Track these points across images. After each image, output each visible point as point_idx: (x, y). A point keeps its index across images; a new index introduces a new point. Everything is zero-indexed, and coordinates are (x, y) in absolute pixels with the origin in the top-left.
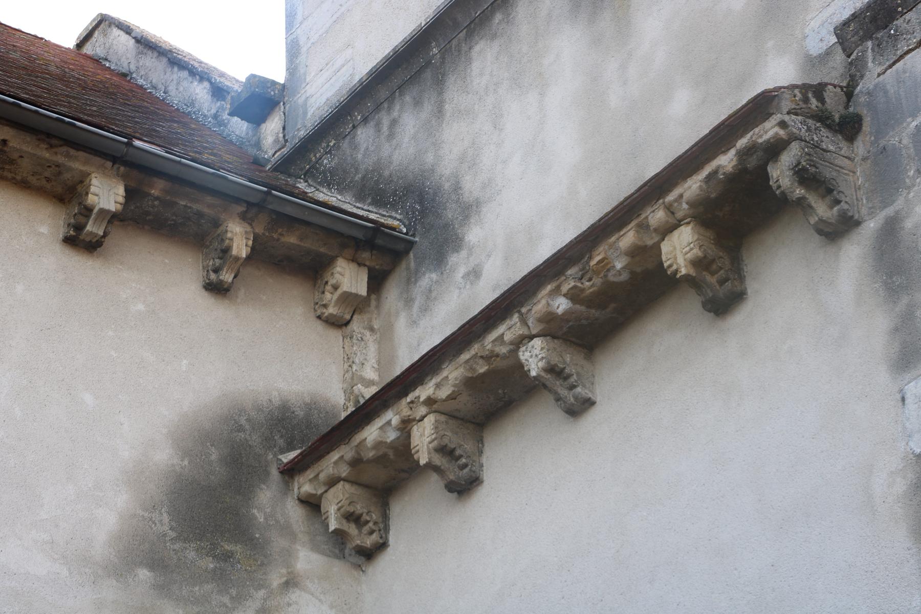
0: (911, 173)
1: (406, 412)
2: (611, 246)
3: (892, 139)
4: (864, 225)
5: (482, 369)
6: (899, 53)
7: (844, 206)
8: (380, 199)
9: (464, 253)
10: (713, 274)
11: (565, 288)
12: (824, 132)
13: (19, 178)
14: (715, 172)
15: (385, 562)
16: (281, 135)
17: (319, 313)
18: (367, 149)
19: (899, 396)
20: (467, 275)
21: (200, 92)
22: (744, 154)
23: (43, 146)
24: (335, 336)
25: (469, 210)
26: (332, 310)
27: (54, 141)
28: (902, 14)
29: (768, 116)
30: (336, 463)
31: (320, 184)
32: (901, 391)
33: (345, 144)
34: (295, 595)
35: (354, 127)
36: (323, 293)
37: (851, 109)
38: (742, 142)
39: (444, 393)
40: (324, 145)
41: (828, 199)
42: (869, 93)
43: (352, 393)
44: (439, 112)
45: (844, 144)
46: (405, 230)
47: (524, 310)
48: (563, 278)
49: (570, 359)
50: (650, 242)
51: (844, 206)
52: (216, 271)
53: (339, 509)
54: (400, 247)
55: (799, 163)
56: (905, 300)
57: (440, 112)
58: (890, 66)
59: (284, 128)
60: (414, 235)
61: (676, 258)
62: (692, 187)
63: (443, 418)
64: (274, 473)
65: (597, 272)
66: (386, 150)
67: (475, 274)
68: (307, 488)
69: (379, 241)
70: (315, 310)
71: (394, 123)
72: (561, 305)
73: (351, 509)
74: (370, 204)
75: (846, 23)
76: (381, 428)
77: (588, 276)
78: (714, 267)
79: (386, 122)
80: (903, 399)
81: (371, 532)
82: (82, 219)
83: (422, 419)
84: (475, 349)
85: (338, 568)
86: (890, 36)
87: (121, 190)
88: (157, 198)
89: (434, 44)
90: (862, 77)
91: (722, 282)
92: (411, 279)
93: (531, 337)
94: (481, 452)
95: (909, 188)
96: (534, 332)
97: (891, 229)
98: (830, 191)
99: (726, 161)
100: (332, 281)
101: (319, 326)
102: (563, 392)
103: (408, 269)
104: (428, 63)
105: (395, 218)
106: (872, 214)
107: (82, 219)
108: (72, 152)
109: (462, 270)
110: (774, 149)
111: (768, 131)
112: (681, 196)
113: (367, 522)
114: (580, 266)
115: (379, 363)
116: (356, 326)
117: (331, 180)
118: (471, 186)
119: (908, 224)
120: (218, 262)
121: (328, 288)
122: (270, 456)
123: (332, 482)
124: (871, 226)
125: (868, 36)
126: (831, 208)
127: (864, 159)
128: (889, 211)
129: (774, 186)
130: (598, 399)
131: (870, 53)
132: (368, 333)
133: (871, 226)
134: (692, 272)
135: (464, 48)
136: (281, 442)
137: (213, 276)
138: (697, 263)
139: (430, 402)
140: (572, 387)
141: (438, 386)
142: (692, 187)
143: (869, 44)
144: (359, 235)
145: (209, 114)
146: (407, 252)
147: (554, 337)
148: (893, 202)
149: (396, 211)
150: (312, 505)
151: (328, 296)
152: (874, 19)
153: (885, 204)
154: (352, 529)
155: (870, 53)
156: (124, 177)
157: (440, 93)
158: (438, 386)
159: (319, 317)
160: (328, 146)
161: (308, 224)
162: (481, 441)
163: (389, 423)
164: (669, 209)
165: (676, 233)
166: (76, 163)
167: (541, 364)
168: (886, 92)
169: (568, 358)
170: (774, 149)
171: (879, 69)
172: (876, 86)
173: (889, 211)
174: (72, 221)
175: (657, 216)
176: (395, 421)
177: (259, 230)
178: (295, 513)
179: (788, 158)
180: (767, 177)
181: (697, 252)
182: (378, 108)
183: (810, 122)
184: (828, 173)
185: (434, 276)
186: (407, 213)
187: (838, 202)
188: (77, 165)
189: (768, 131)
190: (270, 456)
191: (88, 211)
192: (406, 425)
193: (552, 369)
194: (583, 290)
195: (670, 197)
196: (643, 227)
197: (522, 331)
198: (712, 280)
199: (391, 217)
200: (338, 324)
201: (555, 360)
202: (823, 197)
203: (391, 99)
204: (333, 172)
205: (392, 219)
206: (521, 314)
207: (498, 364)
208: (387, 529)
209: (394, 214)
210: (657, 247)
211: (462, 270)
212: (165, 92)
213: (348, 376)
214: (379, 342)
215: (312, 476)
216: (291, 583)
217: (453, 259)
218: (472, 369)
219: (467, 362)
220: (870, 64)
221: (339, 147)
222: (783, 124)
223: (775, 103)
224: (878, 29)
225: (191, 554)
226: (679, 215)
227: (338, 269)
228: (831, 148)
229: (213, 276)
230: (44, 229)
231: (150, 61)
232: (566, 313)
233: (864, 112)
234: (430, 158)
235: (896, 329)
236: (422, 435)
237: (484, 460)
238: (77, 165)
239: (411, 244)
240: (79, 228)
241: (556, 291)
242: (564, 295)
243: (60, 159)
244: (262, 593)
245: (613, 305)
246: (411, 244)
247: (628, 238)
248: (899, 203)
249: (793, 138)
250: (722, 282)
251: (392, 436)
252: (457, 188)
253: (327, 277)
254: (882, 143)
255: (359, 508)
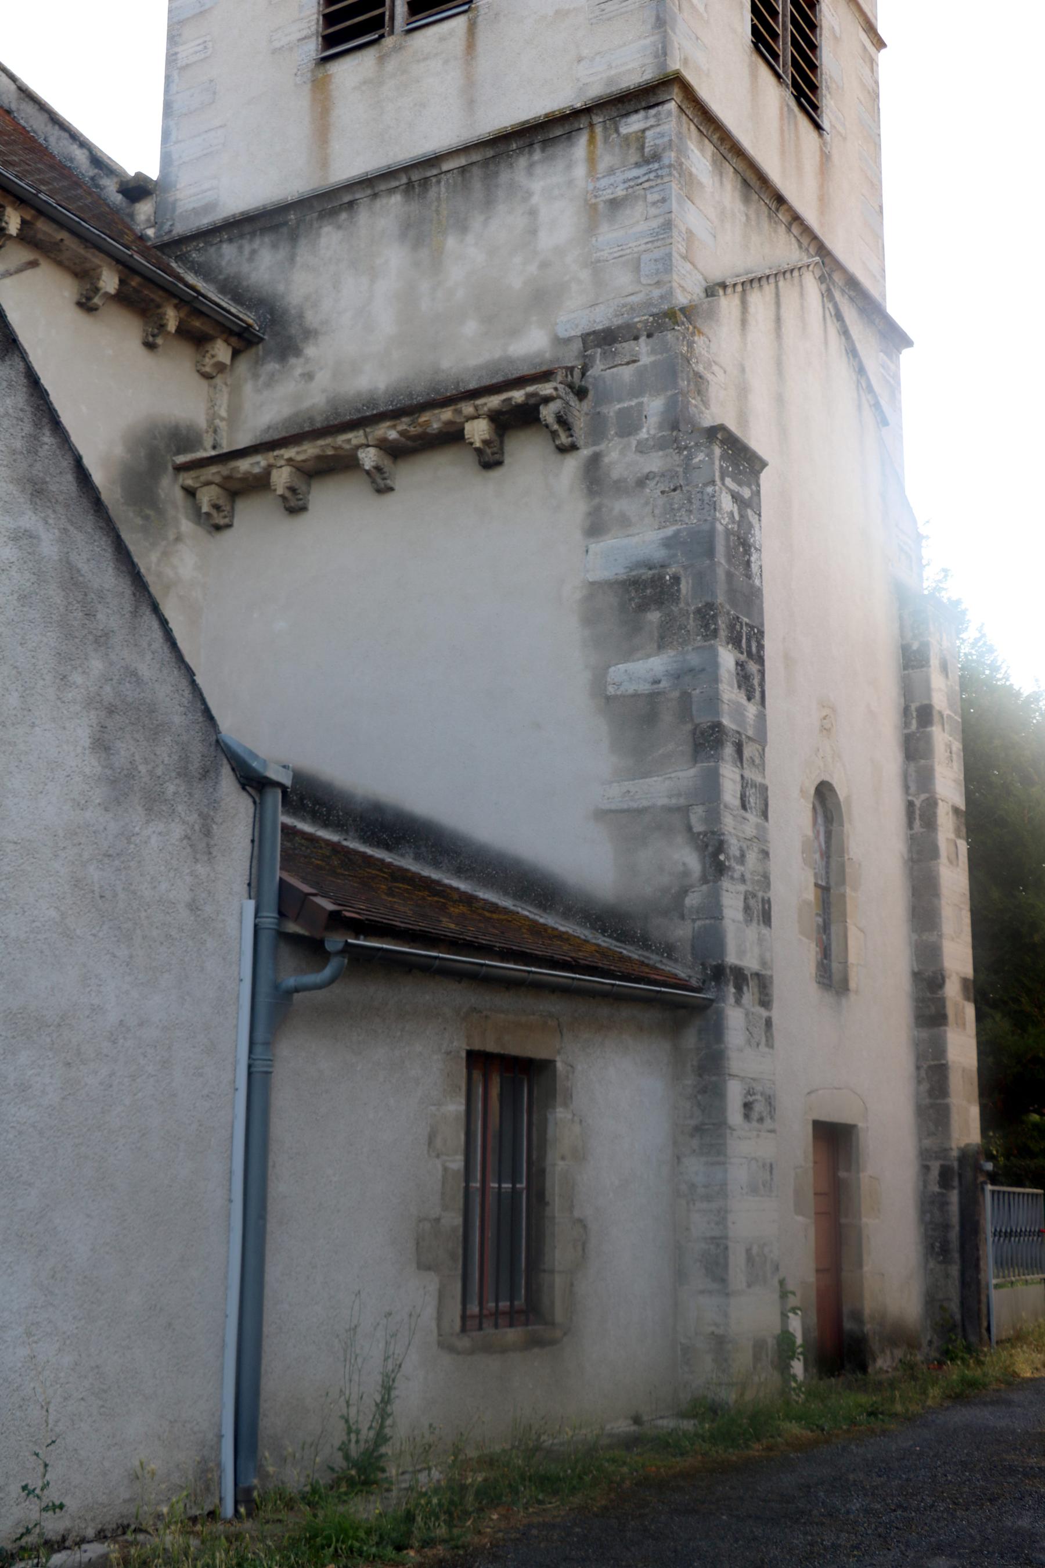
0: (612, 433)
1: (272, 461)
2: (434, 415)
3: (604, 410)
4: (581, 451)
5: (330, 452)
6: (615, 363)
7: (574, 439)
8: (238, 298)
9: (301, 360)
10: (489, 448)
11: (400, 428)
12: (571, 395)
13: (58, 259)
14: (509, 399)
15: (227, 535)
16: (152, 218)
17: (198, 368)
18: (230, 261)
19: (585, 549)
20: (303, 375)
21: (80, 156)
22: (529, 396)
23: (82, 246)
24: (204, 383)
25: (309, 334)
26: (208, 369)
27: (89, 245)
28: (620, 342)
29: (548, 381)
30: (214, 474)
31: (188, 269)
32: (587, 546)
33: (212, 250)
34: (180, 546)
35: (221, 241)
36: (204, 357)
37: (583, 383)
38: (530, 389)
39: (300, 458)
40: (194, 244)
41: (567, 433)
42: (595, 378)
43: (213, 423)
44: (292, 259)
45: (577, 402)
46: (257, 328)
47: (368, 430)
48: (398, 421)
49: (387, 463)
50: (458, 420)
51: (574, 439)
52: (153, 336)
53: (210, 501)
54: (256, 340)
55: (559, 412)
56: (597, 500)
57: (292, 260)
58: (610, 368)
59: (155, 213)
60: (263, 334)
61: (473, 435)
62: (494, 401)
63: (294, 470)
64: (170, 468)
65: (420, 425)
66: (245, 268)
67: (309, 376)
68: (189, 482)
69: (246, 335)
70: (196, 366)
71: (254, 252)
72: (393, 435)
73: (217, 502)
74: (229, 299)
75: (588, 334)
76: (252, 464)
77: (414, 425)
78: (492, 445)
79: (247, 249)
80: (587, 551)
81: (225, 517)
82: (91, 294)
83: (281, 467)
84: (329, 440)
85: (201, 532)
86: (611, 351)
87: (116, 281)
88: (133, 287)
89: (292, 212)
90: (592, 367)
91: (493, 454)
92: (258, 362)
93: (368, 446)
94: (309, 493)
95: (610, 441)
96: (370, 443)
97: (595, 460)
98: (569, 429)
99: (518, 396)
100: (212, 352)
101: (196, 376)
102: (379, 481)
103: (257, 354)
104: (286, 223)
105: (249, 317)
106: (586, 445)
107: (91, 294)
108: (97, 253)
109: (299, 371)
110: (547, 400)
111: (546, 389)
112: (485, 404)
113: (224, 511)
114: (411, 418)
115: (229, 406)
116: (219, 380)
117: (197, 269)
118: (311, 318)
119: (606, 460)
120: (156, 331)
121: (208, 355)
122: (169, 457)
123: (208, 483)
124: (585, 452)
125: (599, 346)
126: (567, 437)
127: (587, 414)
128: (596, 449)
129: (542, 419)
130: (396, 487)
131: (598, 355)
132: (224, 386)
133: (585, 452)
134: (482, 447)
135: (316, 225)
136: (174, 449)
137: (151, 339)
138: (485, 442)
139: (290, 460)
140: (384, 479)
141: (298, 453)
142: (494, 401)
143: (599, 350)
144: (236, 329)
145: (87, 174)
146: (258, 343)
147: (381, 449)
148: (599, 444)
149: (251, 312)
150: (190, 493)
151: (207, 360)
152: (604, 338)
153: (595, 444)
154: (214, 513)
155: (598, 355)
156: (120, 272)
157: (294, 247)
158: (298, 453)
159: (198, 371)
160: (198, 246)
161: (208, 316)
162: (309, 485)
163: (258, 463)
164: (476, 408)
165: (476, 421)
166: (96, 259)
167: (373, 464)
168: (604, 382)
169: (386, 462)
170: (547, 400)
171: (602, 367)
172: (600, 376)
173: (596, 449)
174: (84, 292)
175: (468, 408)
176: (263, 463)
177: (182, 315)
178: (179, 494)
179: (553, 407)
180: (538, 412)
181: (487, 437)
182: (242, 236)
183: (567, 388)
184: (570, 420)
185: (277, 366)
186: (260, 317)
187: (572, 436)
188: (97, 261)
189: (546, 389)
190: (169, 457)
191: (97, 290)
192: (270, 468)
193: (378, 469)
194: (408, 432)
195: (479, 402)
196: (459, 412)
197: (364, 441)
198: (489, 451)
199: (245, 314)
200: (207, 377)
201: (380, 463)
202: (565, 431)
203: (253, 234)
204: (200, 265)
205: (249, 318)
206: (365, 431)
207: (341, 452)
208: (232, 516)
209: (249, 314)
210: (463, 424)
211: (299, 371)
212: (45, 140)
213: (211, 412)
214: (230, 393)
215: (194, 476)
216: (178, 539)
217: (293, 361)
218: (323, 451)
219: (322, 446)
220: (598, 362)
221: (206, 250)
222: (556, 389)
223: (554, 376)
224: (605, 344)
225: (131, 514)
226: (481, 412)
227: (218, 346)
228: (573, 404)
229: (151, 339)
230: (67, 294)
231: (29, 109)
232: (395, 440)
233: (590, 387)
234: (281, 288)
235: (590, 514)
236: (280, 477)
237: (310, 497)
238: (97, 261)
239: (261, 340)
240: (89, 299)
241: (394, 427)
242: (398, 432)
243: (89, 255)
244: (164, 543)
245: (420, 442)
246: (261, 340)
247: (447, 414)
248: (602, 447)
249: (559, 397)
250: (493, 454)
251: (257, 470)
252: (301, 316)
253: (208, 347)
254: (598, 410)
255: (221, 502)
